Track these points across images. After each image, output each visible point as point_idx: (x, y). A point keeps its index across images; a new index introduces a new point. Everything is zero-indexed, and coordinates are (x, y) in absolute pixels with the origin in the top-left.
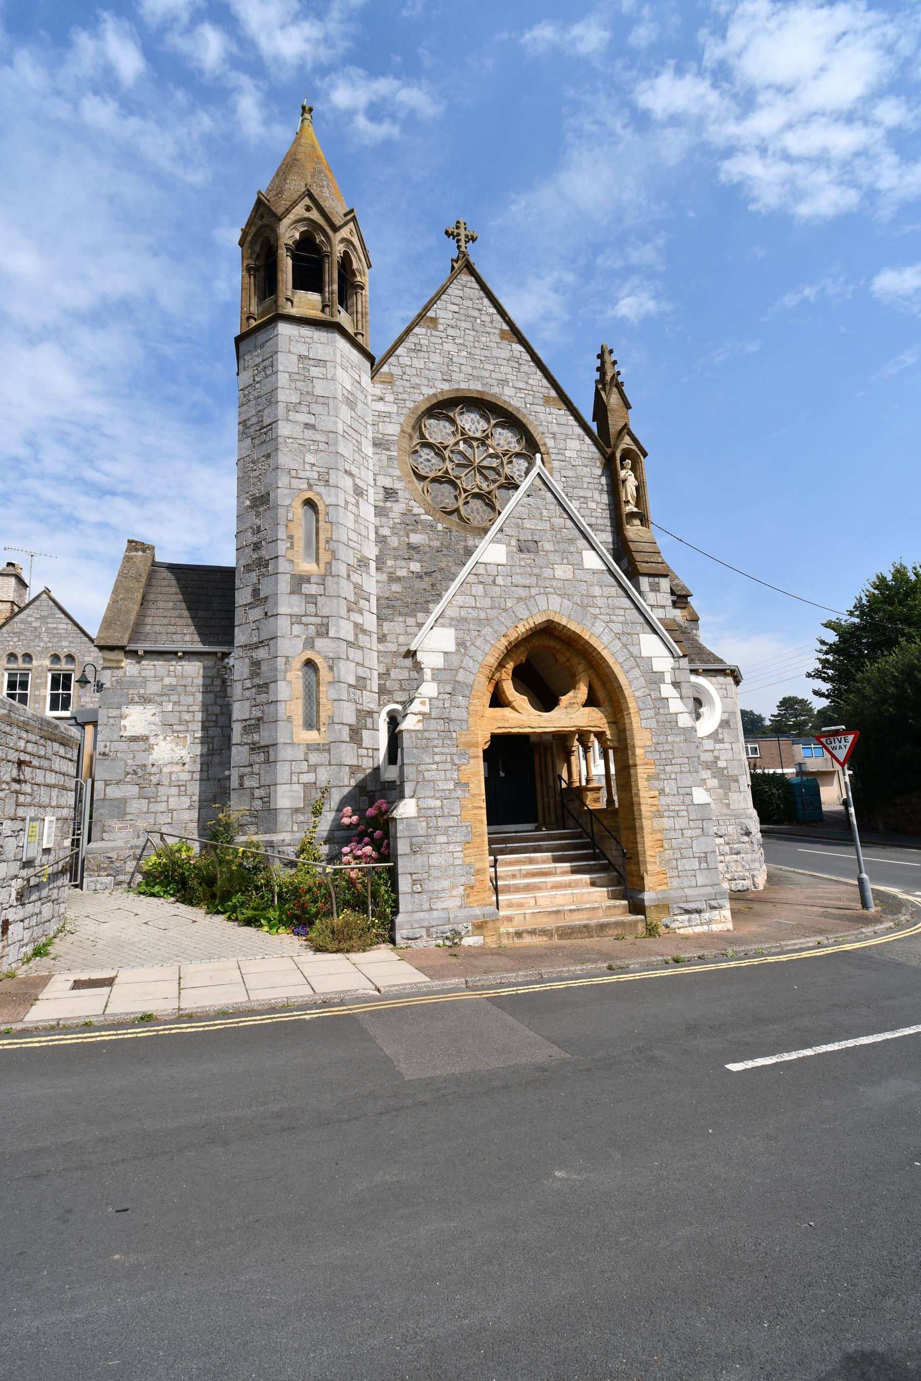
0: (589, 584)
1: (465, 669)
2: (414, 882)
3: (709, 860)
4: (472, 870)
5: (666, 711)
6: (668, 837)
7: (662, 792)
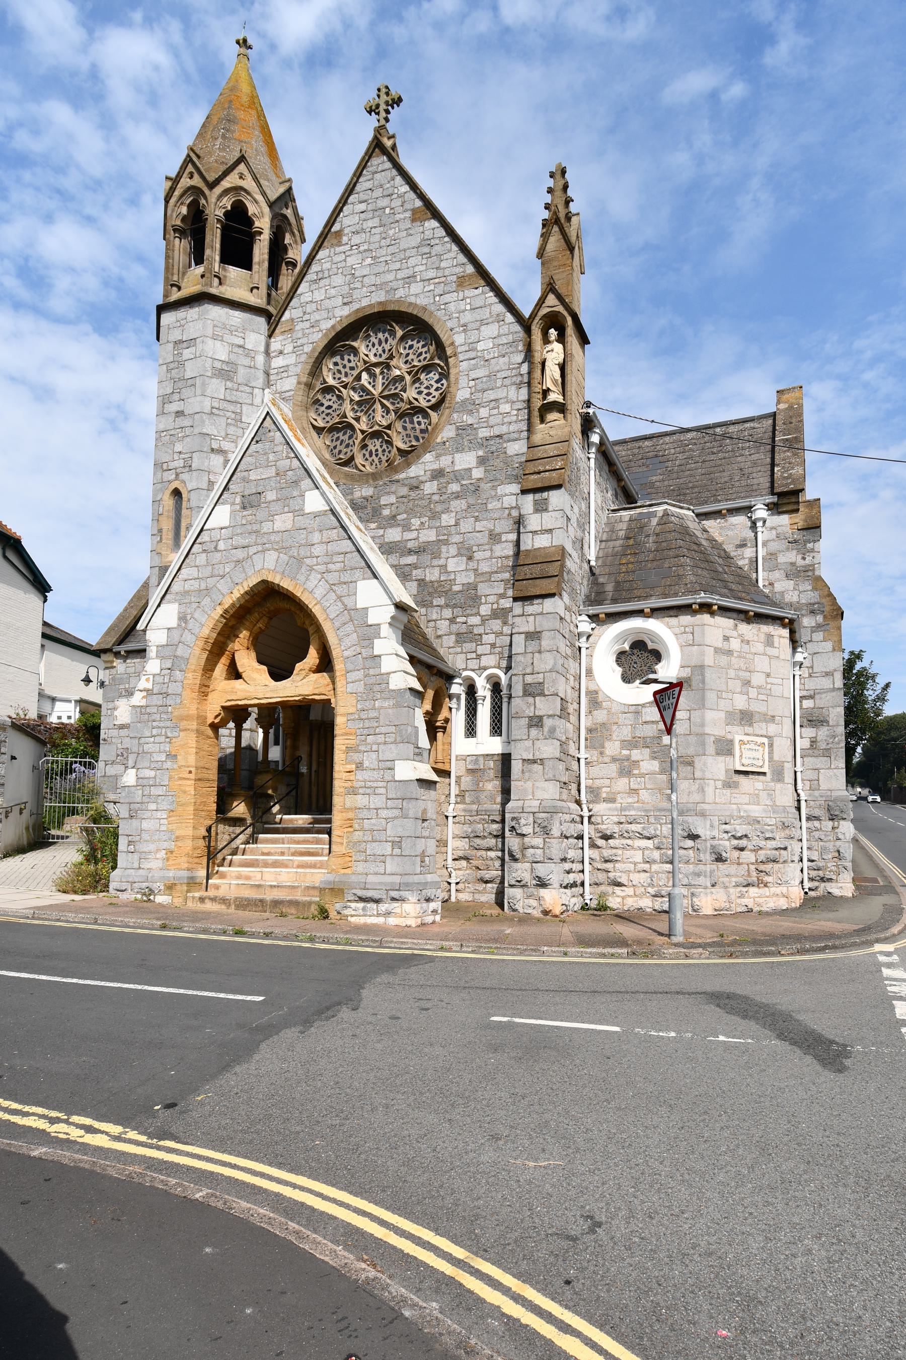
0: (309, 530)
1: (183, 643)
2: (130, 843)
3: (403, 846)
4: (173, 837)
5: (376, 671)
6: (361, 816)
7: (360, 766)
